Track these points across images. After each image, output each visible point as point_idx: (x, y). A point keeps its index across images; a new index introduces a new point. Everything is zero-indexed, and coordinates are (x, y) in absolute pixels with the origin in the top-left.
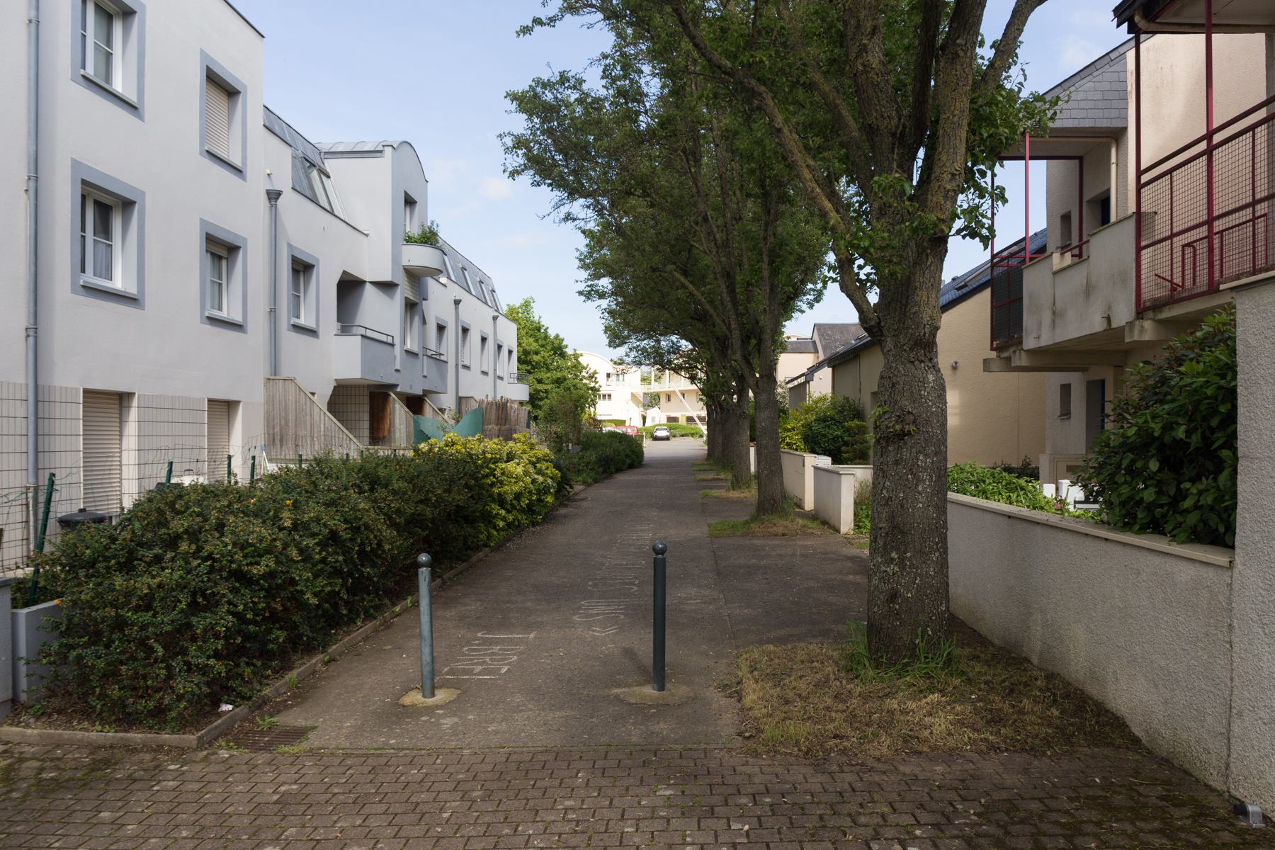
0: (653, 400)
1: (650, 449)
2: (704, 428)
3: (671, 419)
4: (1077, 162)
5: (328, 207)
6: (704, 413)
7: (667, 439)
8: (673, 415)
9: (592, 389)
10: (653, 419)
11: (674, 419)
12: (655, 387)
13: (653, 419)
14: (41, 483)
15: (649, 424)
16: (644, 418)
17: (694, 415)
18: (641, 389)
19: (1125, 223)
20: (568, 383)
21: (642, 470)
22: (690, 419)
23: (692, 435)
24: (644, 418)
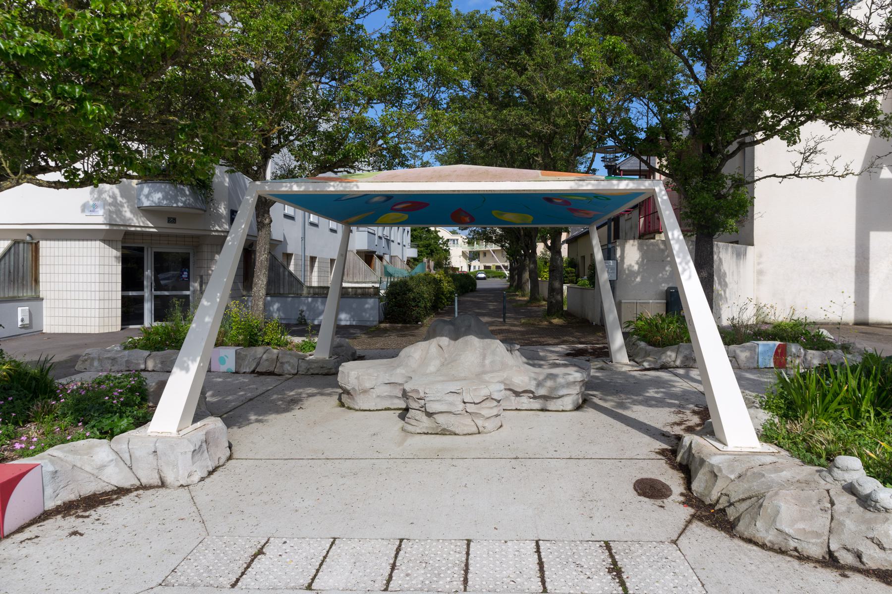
0: (473, 256)
1: (480, 285)
2: (507, 273)
3: (486, 267)
4: (160, 484)
5: (129, 463)
6: (507, 264)
7: (484, 279)
8: (487, 265)
9: (445, 250)
10: (475, 267)
11: (489, 267)
12: (476, 248)
13: (475, 267)
14: (98, 220)
15: (472, 270)
16: (470, 266)
17: (500, 264)
18: (467, 249)
19: (14, 529)
20: (432, 247)
21: (475, 294)
22: (498, 267)
23: (499, 277)
24: (470, 266)
